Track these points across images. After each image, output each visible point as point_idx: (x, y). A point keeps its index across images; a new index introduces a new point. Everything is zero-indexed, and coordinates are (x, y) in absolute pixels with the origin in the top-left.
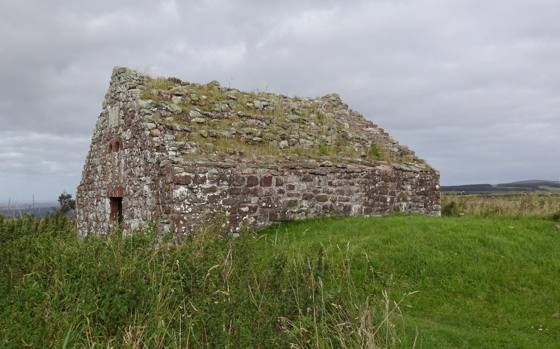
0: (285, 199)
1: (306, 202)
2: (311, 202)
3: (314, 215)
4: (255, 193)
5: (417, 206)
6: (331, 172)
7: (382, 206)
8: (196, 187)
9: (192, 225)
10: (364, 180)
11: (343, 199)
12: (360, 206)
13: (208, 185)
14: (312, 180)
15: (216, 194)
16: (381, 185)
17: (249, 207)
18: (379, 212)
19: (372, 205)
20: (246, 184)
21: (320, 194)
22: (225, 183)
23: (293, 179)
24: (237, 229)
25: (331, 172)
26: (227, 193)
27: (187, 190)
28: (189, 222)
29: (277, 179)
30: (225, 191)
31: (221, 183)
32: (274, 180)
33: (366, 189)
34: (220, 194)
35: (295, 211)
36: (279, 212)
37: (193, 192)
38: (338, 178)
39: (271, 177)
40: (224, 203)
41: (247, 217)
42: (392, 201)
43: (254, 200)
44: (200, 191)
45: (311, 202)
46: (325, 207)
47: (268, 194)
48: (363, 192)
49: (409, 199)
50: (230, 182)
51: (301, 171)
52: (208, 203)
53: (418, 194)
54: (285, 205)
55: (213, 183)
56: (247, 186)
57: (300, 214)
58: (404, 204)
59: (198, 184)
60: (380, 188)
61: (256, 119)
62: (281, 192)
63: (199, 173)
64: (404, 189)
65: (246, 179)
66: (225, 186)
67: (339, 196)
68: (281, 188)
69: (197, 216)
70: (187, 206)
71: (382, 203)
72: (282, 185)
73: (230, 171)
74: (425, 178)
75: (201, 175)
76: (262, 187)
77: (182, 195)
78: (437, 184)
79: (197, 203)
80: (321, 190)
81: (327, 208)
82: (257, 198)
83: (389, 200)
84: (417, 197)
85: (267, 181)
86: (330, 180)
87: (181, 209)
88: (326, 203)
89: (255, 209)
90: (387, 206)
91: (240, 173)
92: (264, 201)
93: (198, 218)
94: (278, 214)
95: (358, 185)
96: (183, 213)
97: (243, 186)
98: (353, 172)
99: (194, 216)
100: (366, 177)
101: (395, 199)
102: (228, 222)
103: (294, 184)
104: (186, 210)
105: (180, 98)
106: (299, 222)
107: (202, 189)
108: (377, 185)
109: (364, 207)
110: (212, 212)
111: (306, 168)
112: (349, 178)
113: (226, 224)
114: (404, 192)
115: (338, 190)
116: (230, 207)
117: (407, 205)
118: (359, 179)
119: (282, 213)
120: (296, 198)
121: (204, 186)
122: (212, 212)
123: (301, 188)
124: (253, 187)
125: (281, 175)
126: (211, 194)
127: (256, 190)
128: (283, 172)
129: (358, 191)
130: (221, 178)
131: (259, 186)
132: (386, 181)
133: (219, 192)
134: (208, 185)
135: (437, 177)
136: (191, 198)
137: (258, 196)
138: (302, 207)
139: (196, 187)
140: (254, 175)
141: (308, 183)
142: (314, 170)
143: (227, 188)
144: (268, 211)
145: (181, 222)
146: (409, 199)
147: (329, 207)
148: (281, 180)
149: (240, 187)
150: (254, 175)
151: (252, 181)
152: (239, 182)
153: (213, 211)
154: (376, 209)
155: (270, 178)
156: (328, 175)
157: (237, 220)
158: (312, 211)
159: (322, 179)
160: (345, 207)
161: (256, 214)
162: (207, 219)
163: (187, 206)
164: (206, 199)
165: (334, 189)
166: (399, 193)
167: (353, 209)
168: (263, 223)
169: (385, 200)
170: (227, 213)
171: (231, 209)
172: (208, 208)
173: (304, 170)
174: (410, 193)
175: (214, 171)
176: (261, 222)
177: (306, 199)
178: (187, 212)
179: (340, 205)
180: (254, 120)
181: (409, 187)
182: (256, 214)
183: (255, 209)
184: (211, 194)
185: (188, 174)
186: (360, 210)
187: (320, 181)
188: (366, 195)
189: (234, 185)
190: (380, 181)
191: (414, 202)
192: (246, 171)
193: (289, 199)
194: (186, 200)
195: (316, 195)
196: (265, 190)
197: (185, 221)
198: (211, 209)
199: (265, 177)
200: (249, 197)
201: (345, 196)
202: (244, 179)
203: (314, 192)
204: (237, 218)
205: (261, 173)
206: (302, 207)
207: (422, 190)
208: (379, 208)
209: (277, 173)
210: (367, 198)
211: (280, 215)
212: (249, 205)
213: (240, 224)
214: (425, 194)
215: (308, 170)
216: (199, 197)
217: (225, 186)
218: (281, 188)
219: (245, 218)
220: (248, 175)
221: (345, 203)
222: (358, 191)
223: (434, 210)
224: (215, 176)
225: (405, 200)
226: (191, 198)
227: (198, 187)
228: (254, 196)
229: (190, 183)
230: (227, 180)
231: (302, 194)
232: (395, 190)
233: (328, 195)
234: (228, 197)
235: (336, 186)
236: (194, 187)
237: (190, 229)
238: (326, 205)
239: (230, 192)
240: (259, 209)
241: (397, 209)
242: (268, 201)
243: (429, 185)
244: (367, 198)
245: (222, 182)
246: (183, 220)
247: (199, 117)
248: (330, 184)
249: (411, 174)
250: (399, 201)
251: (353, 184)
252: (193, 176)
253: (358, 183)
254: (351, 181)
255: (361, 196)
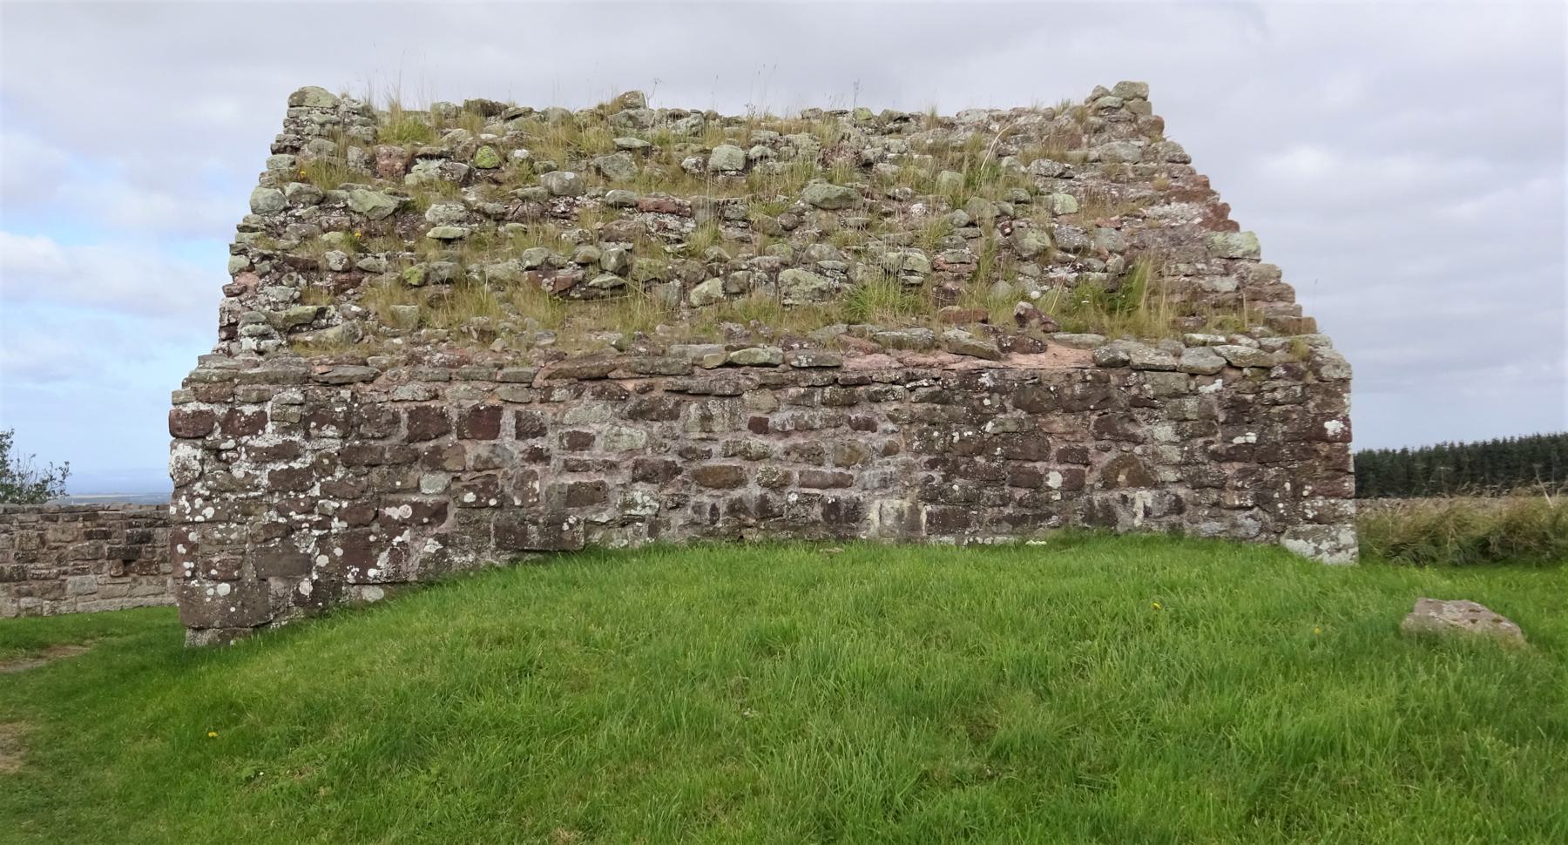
0: (548, 481)
1: (648, 487)
2: (671, 490)
3: (690, 532)
4: (435, 462)
5: (1216, 504)
6: (762, 386)
7: (1020, 503)
8: (231, 444)
9: (216, 559)
10: (919, 408)
11: (818, 479)
12: (906, 504)
13: (269, 437)
14: (673, 415)
15: (296, 465)
16: (1011, 427)
17: (414, 505)
18: (1007, 527)
19: (970, 501)
20: (404, 432)
21: (713, 462)
22: (330, 431)
23: (591, 414)
24: (372, 572)
25: (762, 386)
26: (333, 463)
27: (199, 453)
28: (207, 549)
29: (518, 415)
30: (328, 456)
31: (314, 432)
32: (508, 419)
33: (931, 441)
34: (313, 466)
35: (604, 518)
36: (535, 523)
37: (220, 460)
38: (795, 403)
39: (499, 409)
40: (327, 492)
41: (407, 536)
42: (1074, 485)
43: (432, 486)
44: (244, 456)
45: (671, 490)
46: (736, 508)
47: (484, 464)
48: (918, 453)
49: (1170, 475)
50: (347, 426)
51: (630, 386)
52: (271, 493)
53: (1216, 456)
54: (555, 498)
55: (287, 430)
56: (410, 440)
57: (629, 530)
58: (1144, 497)
59: (237, 435)
60: (1006, 437)
61: (658, 209)
62: (537, 456)
63: (243, 403)
64: (1135, 440)
65: (405, 416)
66: (330, 440)
67: (804, 467)
68: (539, 443)
69: (233, 531)
70: (198, 502)
71: (1020, 493)
72: (541, 432)
73: (346, 393)
74: (1258, 391)
75: (249, 410)
76: (464, 442)
77: (185, 468)
78: (1331, 417)
79: (233, 491)
80: (716, 448)
81: (746, 511)
82: (442, 479)
83: (1055, 480)
84: (1212, 467)
85: (483, 423)
86: (757, 414)
87: (180, 512)
88: (737, 493)
89: (439, 513)
90: (1048, 502)
91: (384, 398)
92: (469, 488)
93: (234, 536)
94: (534, 528)
95: (890, 426)
96: (187, 523)
97: (394, 440)
98: (862, 382)
99: (221, 532)
100: (932, 398)
101: (1092, 478)
102: (339, 552)
103: (592, 429)
104: (195, 512)
105: (436, 163)
106: (622, 555)
107: (249, 449)
108: (989, 426)
109: (926, 509)
110: (281, 520)
111: (651, 375)
112: (851, 405)
113: (333, 559)
114: (1138, 450)
115: (795, 447)
116: (345, 504)
117: (1159, 500)
118: (896, 405)
119: (549, 524)
120: (602, 478)
121: (257, 443)
122: (281, 520)
123: (624, 444)
124: (431, 444)
125: (542, 402)
126: (282, 466)
127: (437, 450)
128: (550, 389)
129: (889, 451)
130: (312, 417)
131: (453, 437)
132: (1033, 409)
133: (309, 459)
134: (269, 437)
135: (1333, 390)
136: (214, 479)
137: (445, 470)
138: (627, 505)
139: (231, 444)
140: (433, 404)
141: (656, 426)
142: (686, 381)
143: (334, 446)
144: (491, 519)
145: (181, 549)
146: (1170, 475)
147: (752, 507)
148: (534, 419)
149: (386, 443)
150: (433, 404)
151: (427, 422)
152: (378, 427)
153: (288, 517)
154: (990, 513)
155: (496, 412)
156: (745, 396)
157: (370, 545)
158: (678, 519)
159: (715, 411)
160: (832, 509)
161: (444, 528)
162: (266, 541)
163: (198, 502)
164: (265, 482)
165: (778, 445)
166: (1108, 457)
167: (873, 515)
168: (471, 558)
169: (1036, 482)
170: (337, 525)
171: (348, 510)
172: (270, 507)
173: (642, 383)
174: (1175, 455)
175: (294, 394)
176: (465, 553)
177: (645, 479)
178: (199, 518)
179: (808, 501)
180: (650, 217)
181: (1164, 431)
182: (444, 528)
183: (439, 513)
184: (282, 466)
185: (204, 407)
186: (909, 524)
187: (706, 418)
188: (932, 465)
189: (360, 437)
190: (1003, 410)
191: (1200, 487)
192: (404, 392)
193: (570, 480)
194: (199, 485)
195: (695, 466)
196: (476, 450)
197: (193, 547)
198: (282, 512)
199: (476, 409)
200: (413, 475)
201: (828, 469)
202: (396, 420)
203: (680, 454)
204: (372, 538)
205: (458, 398)
206: (632, 504)
207: (1238, 440)
208: (1008, 511)
209: (522, 395)
210: (937, 475)
211: (541, 533)
212: (414, 499)
213: (383, 560)
214: (1261, 455)
215: (663, 381)
216: (238, 473)
217: (330, 440)
218: (539, 443)
219: (398, 539)
220: (413, 406)
221: (830, 495)
222: (889, 451)
223: (1310, 521)
224: (294, 409)
225: (1142, 479)
226: (214, 479)
227: (239, 444)
228: (432, 471)
229: (210, 432)
230: (333, 422)
231: (630, 463)
232: (1091, 445)
233: (746, 465)
234: (339, 475)
235: (787, 434)
236: (223, 446)
237: (208, 571)
238: (740, 500)
239: (348, 458)
240: (453, 511)
241: (1107, 517)
242: (486, 487)
243: (1285, 419)
244: (937, 475)
245: (318, 427)
246: (186, 543)
247: (450, 222)
248: (759, 426)
249: (1176, 382)
250: (1109, 484)
251: (869, 426)
252: (220, 411)
253: (893, 419)
254: (858, 414)
255: (908, 468)
